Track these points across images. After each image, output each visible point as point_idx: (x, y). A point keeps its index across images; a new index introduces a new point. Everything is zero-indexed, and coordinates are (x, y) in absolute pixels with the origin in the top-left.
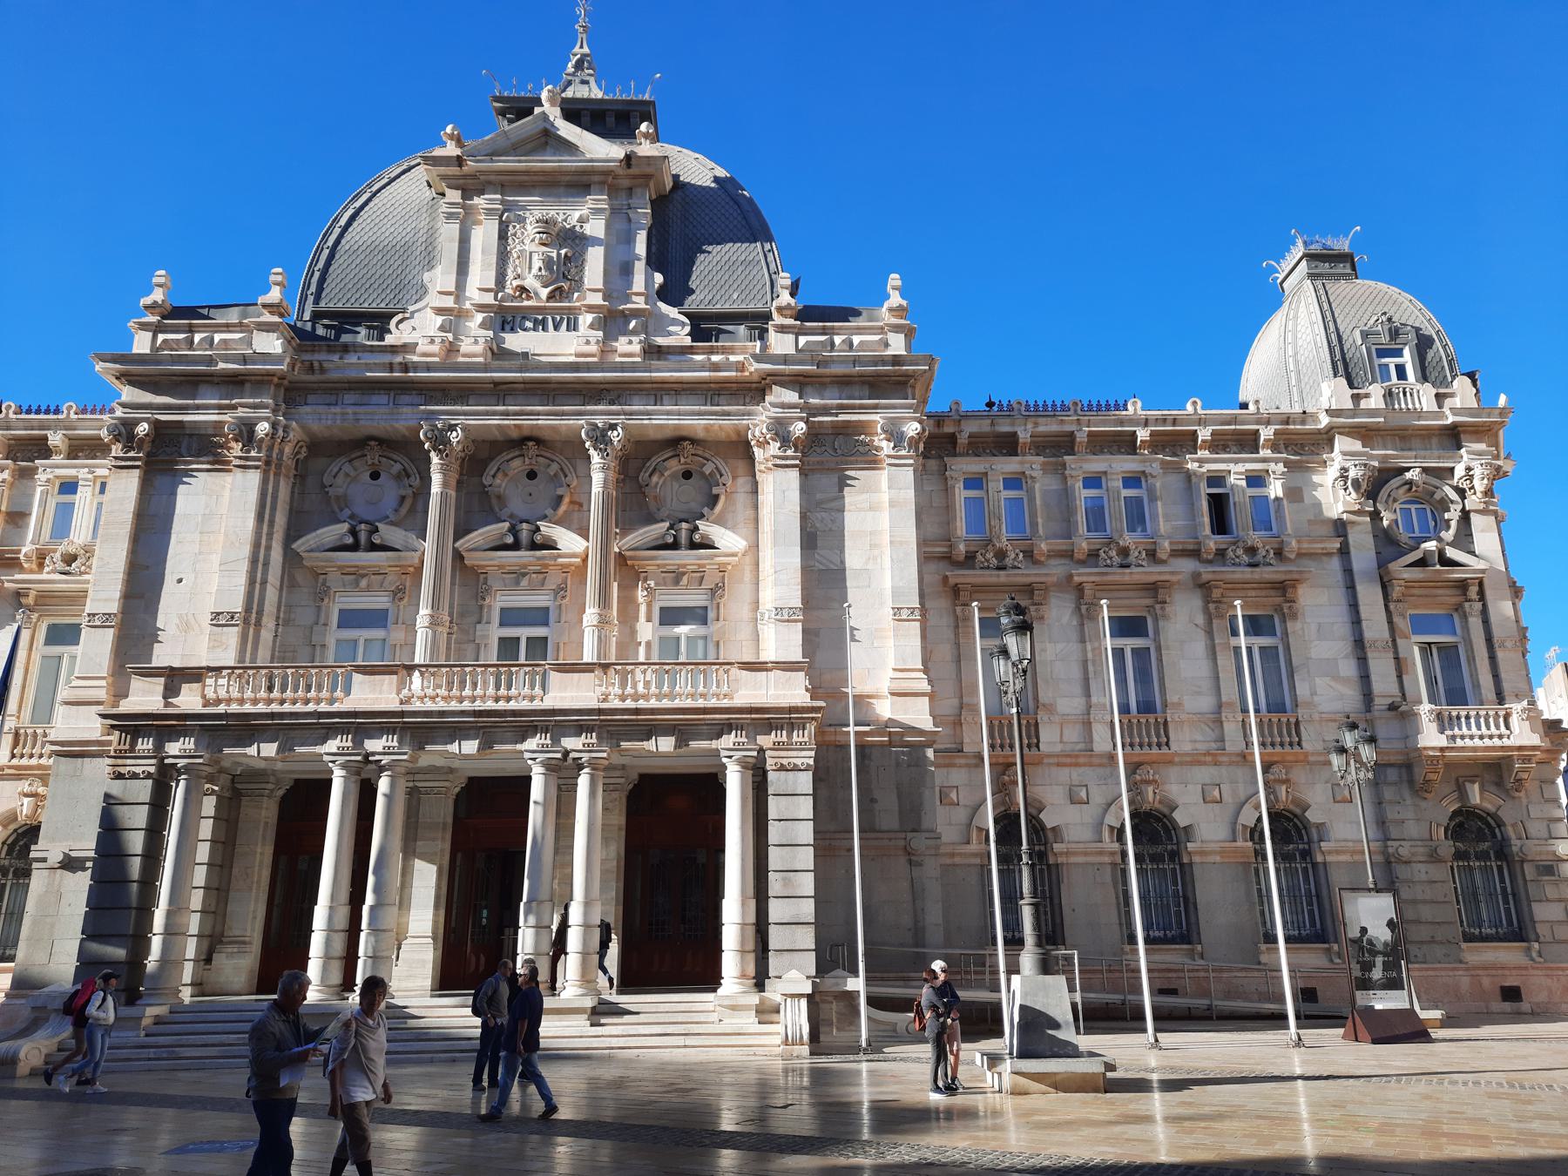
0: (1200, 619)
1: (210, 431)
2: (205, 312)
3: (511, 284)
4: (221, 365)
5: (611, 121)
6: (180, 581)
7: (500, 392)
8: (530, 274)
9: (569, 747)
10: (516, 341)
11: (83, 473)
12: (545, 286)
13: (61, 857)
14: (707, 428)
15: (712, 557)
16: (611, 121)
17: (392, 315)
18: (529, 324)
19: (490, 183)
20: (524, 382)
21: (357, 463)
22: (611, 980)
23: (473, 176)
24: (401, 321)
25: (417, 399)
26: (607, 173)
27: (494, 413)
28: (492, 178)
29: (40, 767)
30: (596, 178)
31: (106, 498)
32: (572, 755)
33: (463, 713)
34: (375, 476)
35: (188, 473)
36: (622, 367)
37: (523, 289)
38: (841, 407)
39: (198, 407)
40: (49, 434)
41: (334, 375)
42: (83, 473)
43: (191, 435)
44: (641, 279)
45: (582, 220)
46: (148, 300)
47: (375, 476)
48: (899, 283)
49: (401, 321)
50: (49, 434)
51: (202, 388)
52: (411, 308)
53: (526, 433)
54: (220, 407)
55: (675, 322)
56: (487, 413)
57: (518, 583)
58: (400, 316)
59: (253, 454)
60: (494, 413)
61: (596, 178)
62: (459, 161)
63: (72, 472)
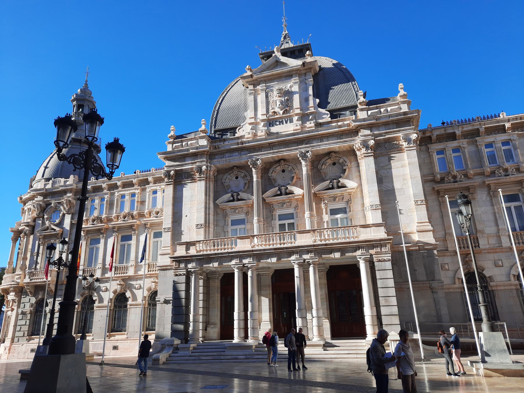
7: (271, 146)
9: (305, 258)
10: (274, 129)
11: (158, 188)
14: (339, 147)
15: (346, 190)
17: (236, 128)
18: (278, 123)
19: (261, 81)
21: (231, 175)
23: (256, 80)
27: (270, 153)
28: (262, 79)
30: (294, 72)
32: (307, 261)
34: (237, 178)
36: (309, 132)
37: (275, 112)
42: (158, 188)
46: (169, 135)
47: (237, 178)
53: (280, 158)
55: (325, 114)
56: (268, 153)
60: (270, 153)
61: (294, 72)
62: (251, 76)
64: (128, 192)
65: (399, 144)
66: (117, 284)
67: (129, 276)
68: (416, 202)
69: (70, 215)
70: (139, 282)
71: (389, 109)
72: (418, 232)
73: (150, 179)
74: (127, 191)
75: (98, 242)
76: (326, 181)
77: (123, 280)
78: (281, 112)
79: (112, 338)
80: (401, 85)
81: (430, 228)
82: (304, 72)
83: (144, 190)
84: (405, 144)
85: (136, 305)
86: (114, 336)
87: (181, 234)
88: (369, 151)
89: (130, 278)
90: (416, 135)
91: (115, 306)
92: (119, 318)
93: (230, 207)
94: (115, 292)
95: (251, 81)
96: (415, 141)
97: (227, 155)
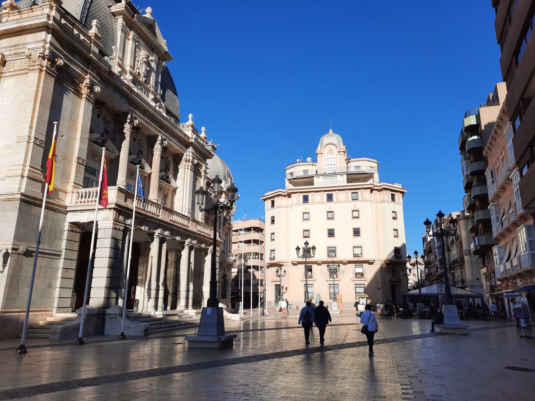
6: (62, 136)
8: (142, 70)
12: (144, 77)
13: (25, 250)
19: (134, 28)
23: (133, 22)
26: (160, 51)
28: (136, 27)
37: (139, 74)
43: (68, 73)
44: (160, 91)
45: (152, 61)
59: (92, 96)
68: (79, 158)
78: (144, 79)
80: (190, 116)
82: (160, 56)
84: (85, 91)
88: (52, 69)
96: (95, 94)
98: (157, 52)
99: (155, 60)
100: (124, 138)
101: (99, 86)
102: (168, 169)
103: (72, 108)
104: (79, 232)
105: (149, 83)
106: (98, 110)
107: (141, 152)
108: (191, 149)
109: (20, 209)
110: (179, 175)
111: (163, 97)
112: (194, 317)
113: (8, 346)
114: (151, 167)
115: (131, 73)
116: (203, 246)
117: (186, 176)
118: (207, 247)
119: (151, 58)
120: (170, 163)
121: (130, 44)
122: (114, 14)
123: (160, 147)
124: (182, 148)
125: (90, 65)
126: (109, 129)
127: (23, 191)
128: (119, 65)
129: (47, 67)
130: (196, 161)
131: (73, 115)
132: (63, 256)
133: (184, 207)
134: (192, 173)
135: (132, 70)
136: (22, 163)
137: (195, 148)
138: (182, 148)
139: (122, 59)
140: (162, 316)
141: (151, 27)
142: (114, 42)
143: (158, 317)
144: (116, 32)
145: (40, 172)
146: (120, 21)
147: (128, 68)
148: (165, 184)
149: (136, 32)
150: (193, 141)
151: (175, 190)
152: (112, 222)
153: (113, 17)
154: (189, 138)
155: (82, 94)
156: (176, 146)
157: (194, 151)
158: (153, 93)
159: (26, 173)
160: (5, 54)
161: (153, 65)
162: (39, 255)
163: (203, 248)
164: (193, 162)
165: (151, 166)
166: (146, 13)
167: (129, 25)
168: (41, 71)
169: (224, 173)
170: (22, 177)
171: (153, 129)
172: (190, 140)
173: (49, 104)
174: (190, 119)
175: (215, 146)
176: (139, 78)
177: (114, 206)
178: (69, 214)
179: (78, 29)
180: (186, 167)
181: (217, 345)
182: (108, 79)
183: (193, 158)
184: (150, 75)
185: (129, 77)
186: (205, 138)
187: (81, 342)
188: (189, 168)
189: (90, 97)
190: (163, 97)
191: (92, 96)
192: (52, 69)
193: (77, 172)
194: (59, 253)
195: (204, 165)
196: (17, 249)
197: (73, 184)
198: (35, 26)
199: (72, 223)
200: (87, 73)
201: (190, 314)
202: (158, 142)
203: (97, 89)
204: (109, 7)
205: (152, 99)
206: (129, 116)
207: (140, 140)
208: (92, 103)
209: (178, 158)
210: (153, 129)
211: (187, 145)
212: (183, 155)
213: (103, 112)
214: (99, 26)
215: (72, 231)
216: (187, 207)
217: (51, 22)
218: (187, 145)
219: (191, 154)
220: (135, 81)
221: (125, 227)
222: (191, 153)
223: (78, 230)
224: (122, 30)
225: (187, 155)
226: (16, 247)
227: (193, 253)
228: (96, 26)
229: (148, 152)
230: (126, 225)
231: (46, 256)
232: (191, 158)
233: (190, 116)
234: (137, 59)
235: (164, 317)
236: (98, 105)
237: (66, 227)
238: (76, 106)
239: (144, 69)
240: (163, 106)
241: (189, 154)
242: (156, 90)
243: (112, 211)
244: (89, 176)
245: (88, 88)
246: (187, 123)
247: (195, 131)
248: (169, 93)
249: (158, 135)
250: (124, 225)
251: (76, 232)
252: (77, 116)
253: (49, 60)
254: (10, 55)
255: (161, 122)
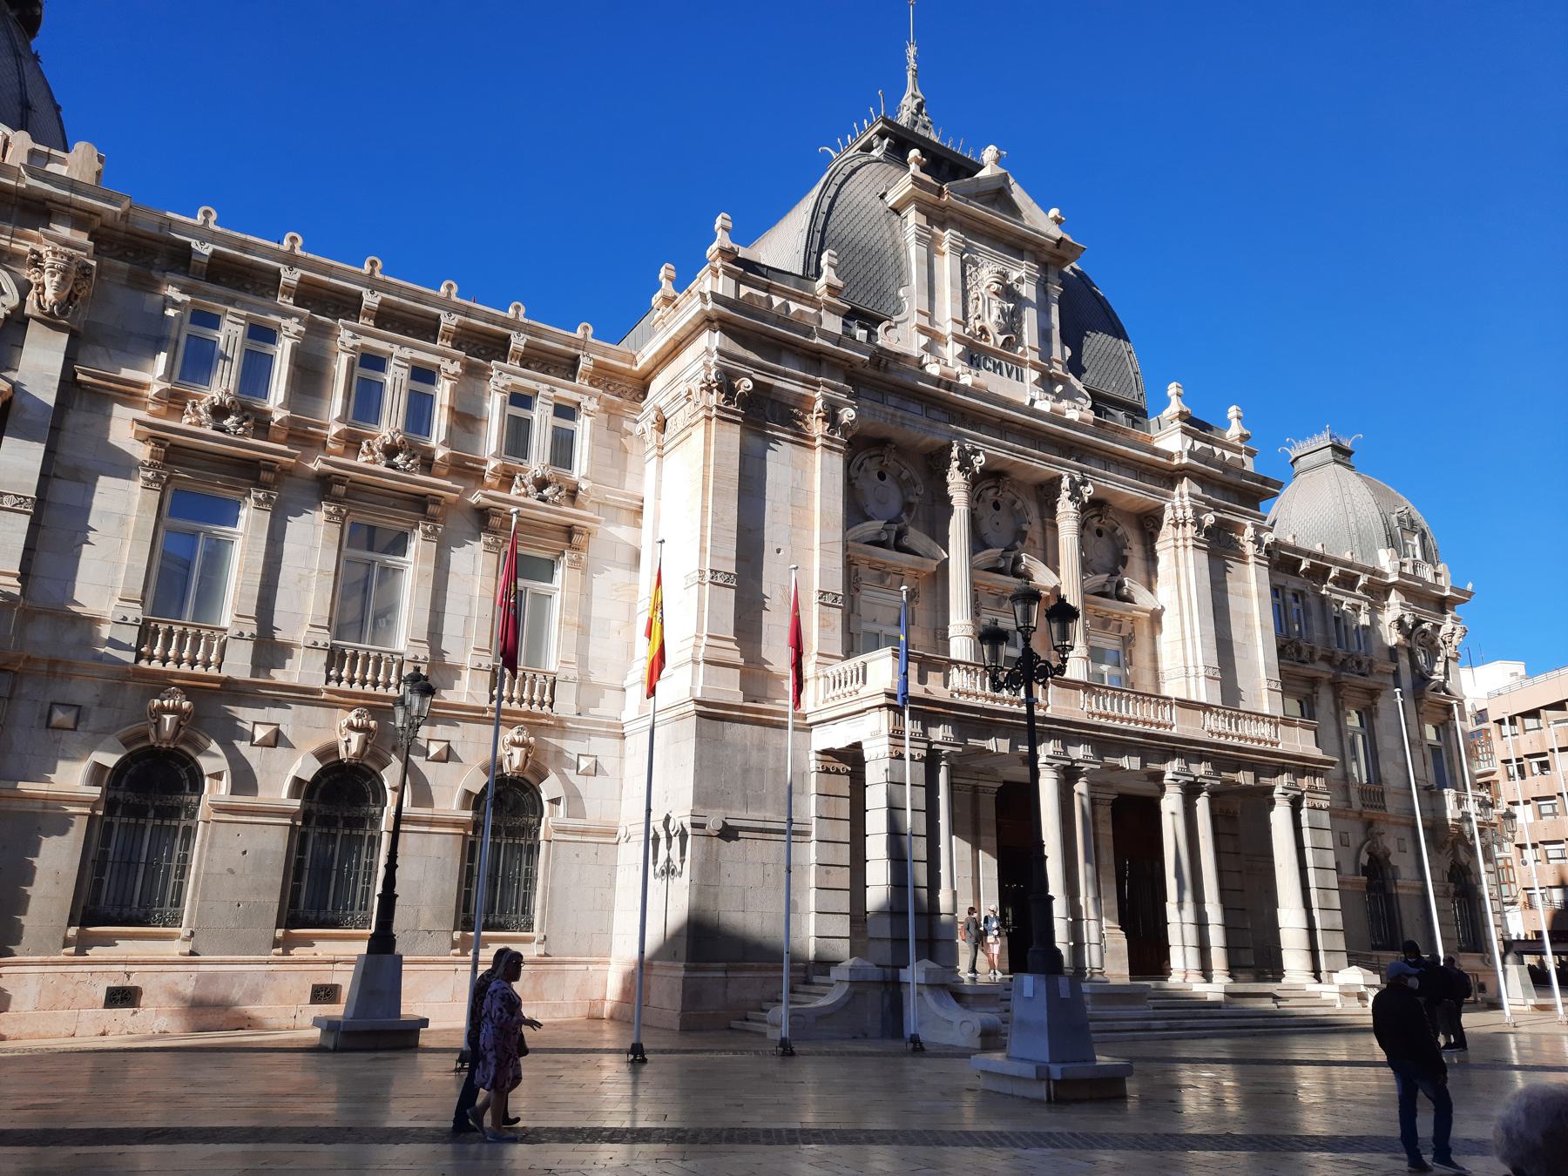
0: (1332, 709)
1: (791, 402)
2: (764, 271)
3: (974, 324)
4: (817, 340)
5: (945, 169)
6: (778, 551)
8: (990, 316)
11: (543, 388)
12: (1001, 333)
13: (720, 826)
15: (1130, 610)
16: (945, 169)
17: (880, 321)
18: (989, 365)
19: (952, 219)
20: (1024, 425)
22: (991, 963)
23: (943, 208)
24: (887, 329)
25: (943, 417)
26: (1040, 246)
27: (1004, 447)
28: (956, 216)
29: (528, 714)
30: (1030, 247)
31: (667, 436)
33: (1137, 734)
35: (775, 439)
37: (983, 330)
38: (1227, 507)
39: (786, 375)
40: (513, 334)
41: (889, 377)
42: (543, 388)
43: (774, 401)
44: (1059, 352)
45: (1020, 281)
47: (882, 476)
48: (673, 274)
49: (887, 329)
50: (513, 334)
51: (785, 356)
52: (896, 318)
54: (805, 380)
55: (1080, 394)
56: (998, 445)
57: (882, 582)
58: (886, 324)
59: (836, 436)
60: (1004, 447)
61: (1030, 247)
63: (531, 384)
64: (406, 353)
65: (1237, 541)
66: (351, 727)
67: (227, 682)
68: (823, 594)
69: (65, 338)
70: (441, 731)
71: (794, 307)
72: (706, 662)
73: (518, 342)
74: (403, 345)
75: (398, 545)
76: (868, 519)
77: (374, 711)
78: (1001, 339)
79: (298, 953)
80: (1173, 389)
81: (741, 661)
82: (1045, 258)
83: (474, 373)
84: (817, 428)
85: (584, 832)
86: (308, 942)
87: (762, 606)
88: (731, 407)
89: (235, 691)
90: (852, 412)
91: (110, 805)
92: (128, 863)
93: (989, 588)
94: (327, 753)
95: (927, 203)
96: (846, 428)
97: (892, 400)
98: (1032, 252)
99: (1030, 276)
100: (950, 510)
101: (851, 406)
102: (1124, 561)
103: (794, 480)
104: (847, 773)
105: (1020, 342)
106: (876, 460)
107: (1021, 535)
108: (1185, 486)
109: (699, 735)
110: (1161, 567)
111: (1075, 366)
112: (1339, 1005)
113: (873, 1050)
114: (1057, 573)
115: (958, 339)
116: (1245, 778)
117: (1182, 570)
118: (1265, 780)
119: (1014, 275)
120: (1121, 539)
121: (947, 266)
122: (896, 210)
123: (1071, 506)
124: (1153, 492)
125: (824, 365)
126: (912, 499)
127: (698, 695)
128: (922, 330)
129: (718, 408)
130: (1209, 519)
131: (799, 494)
132: (813, 837)
133: (1190, 663)
134: (1204, 556)
135: (959, 330)
136: (694, 632)
137: (1202, 479)
138: (1153, 492)
139: (930, 314)
140: (1221, 997)
141: (999, 196)
142: (901, 278)
143: (1211, 997)
144: (906, 251)
145: (732, 645)
146: (912, 217)
147: (947, 328)
148: (1112, 606)
149: (960, 226)
150: (1185, 460)
151: (1156, 617)
152: (886, 740)
153: (895, 217)
154: (1170, 456)
155: (814, 440)
156: (1127, 490)
157: (1198, 490)
158: (1034, 366)
159: (700, 658)
160: (662, 404)
161: (1028, 291)
162: (793, 838)
163: (1247, 788)
164: (1198, 523)
165: (1054, 566)
166: (982, 167)
167: (937, 217)
168: (709, 418)
169: (1386, 523)
170: (695, 662)
171: (1040, 464)
172: (1176, 462)
173: (734, 488)
174: (1174, 399)
175: (1347, 444)
176: (987, 340)
177: (882, 700)
178: (816, 731)
179: (782, 292)
180: (1180, 543)
181: (1040, 1091)
182: (882, 378)
183: (1197, 511)
184: (1021, 320)
185: (952, 350)
186: (1244, 438)
187: (786, 1050)
188: (1190, 543)
189: (832, 440)
190: (1075, 366)
191: (836, 436)
192: (731, 407)
193: (823, 626)
194: (804, 828)
195: (1248, 523)
196: (702, 826)
197: (815, 658)
198: (691, 327)
199: (825, 752)
200: (817, 384)
201: (1325, 996)
202: (1065, 495)
203: (847, 415)
204: (882, 197)
205: (1035, 383)
206: (955, 453)
207: (1014, 503)
208: (840, 451)
209: (1149, 523)
210: (1040, 464)
211: (1168, 477)
212: (1161, 509)
213: (890, 462)
214: (835, 262)
215: (827, 771)
216: (1200, 663)
217: (710, 306)
218: (1168, 477)
219: (1187, 501)
220: (974, 355)
221: (929, 750)
222: (1186, 498)
223: (841, 766)
224: (919, 239)
225: (1174, 508)
226: (698, 820)
227: (1202, 804)
228: (830, 265)
229: (1044, 530)
230: (930, 744)
231: (774, 836)
232: (1189, 513)
233: (1173, 389)
234: (972, 295)
235: (1226, 1002)
236: (860, 449)
237: (813, 765)
238: (803, 470)
239: (995, 312)
240: (1079, 386)
241: (1181, 500)
242: (1045, 353)
243: (885, 711)
244: (1282, 579)
245: (824, 420)
246: (1166, 413)
247: (1195, 425)
248: (1097, 342)
249: (1061, 477)
250: (925, 745)
251: (838, 772)
252: (809, 494)
253: (720, 389)
254: (668, 404)
255: (1063, 437)
